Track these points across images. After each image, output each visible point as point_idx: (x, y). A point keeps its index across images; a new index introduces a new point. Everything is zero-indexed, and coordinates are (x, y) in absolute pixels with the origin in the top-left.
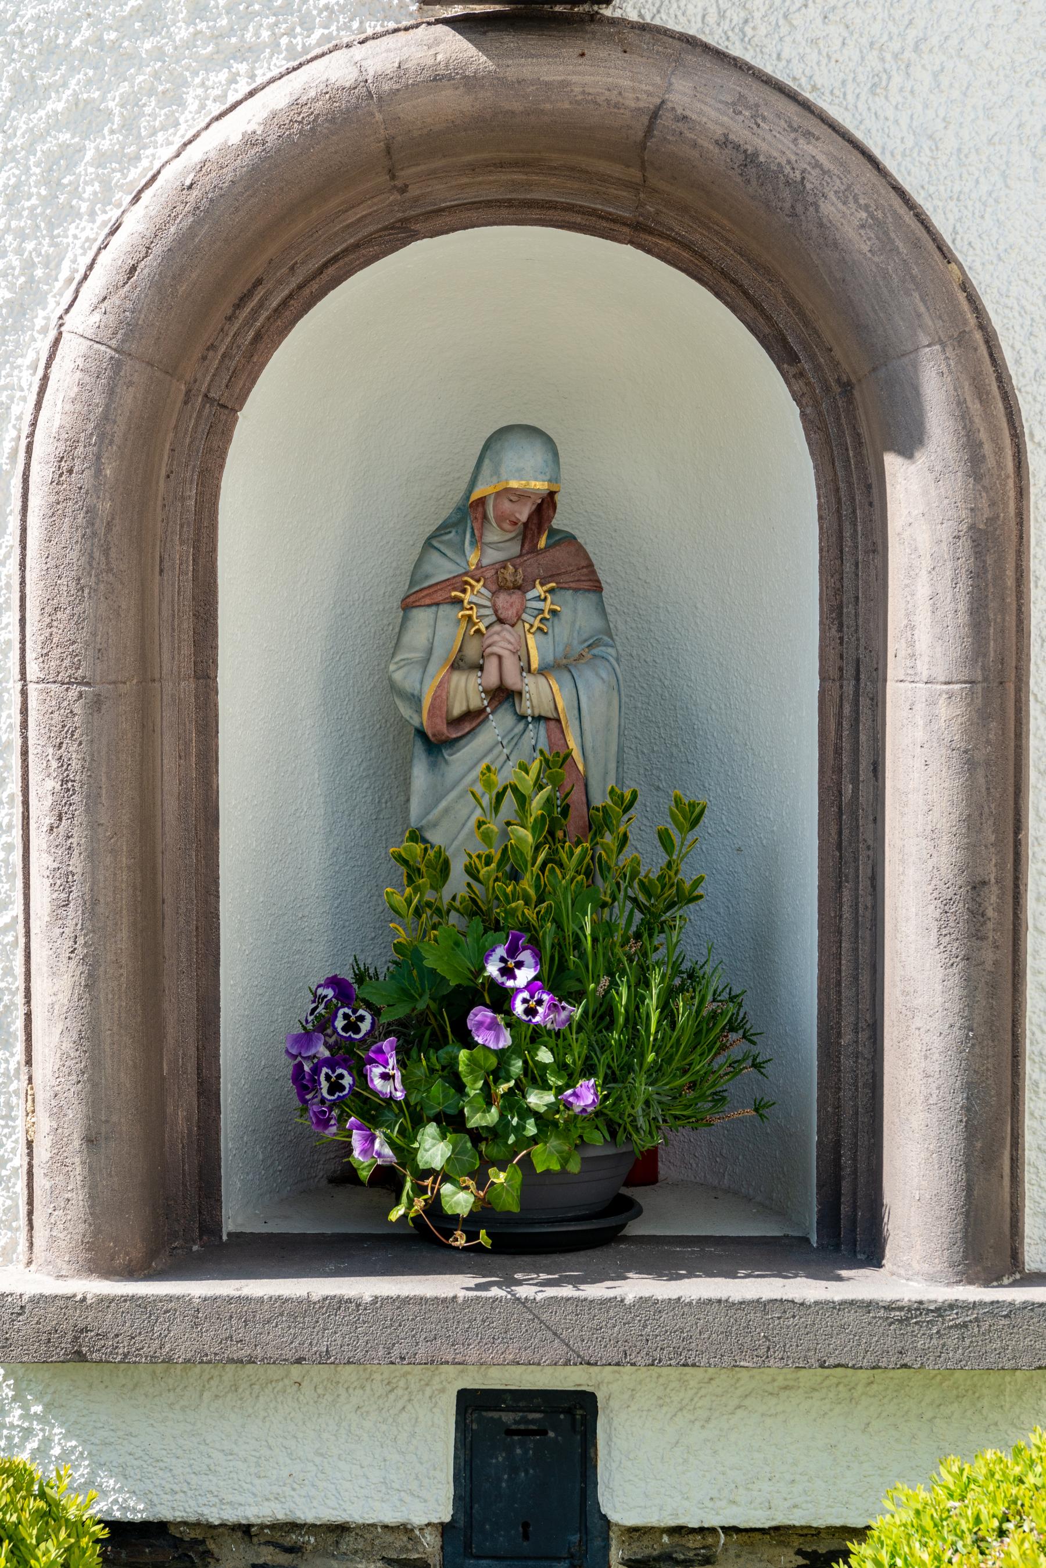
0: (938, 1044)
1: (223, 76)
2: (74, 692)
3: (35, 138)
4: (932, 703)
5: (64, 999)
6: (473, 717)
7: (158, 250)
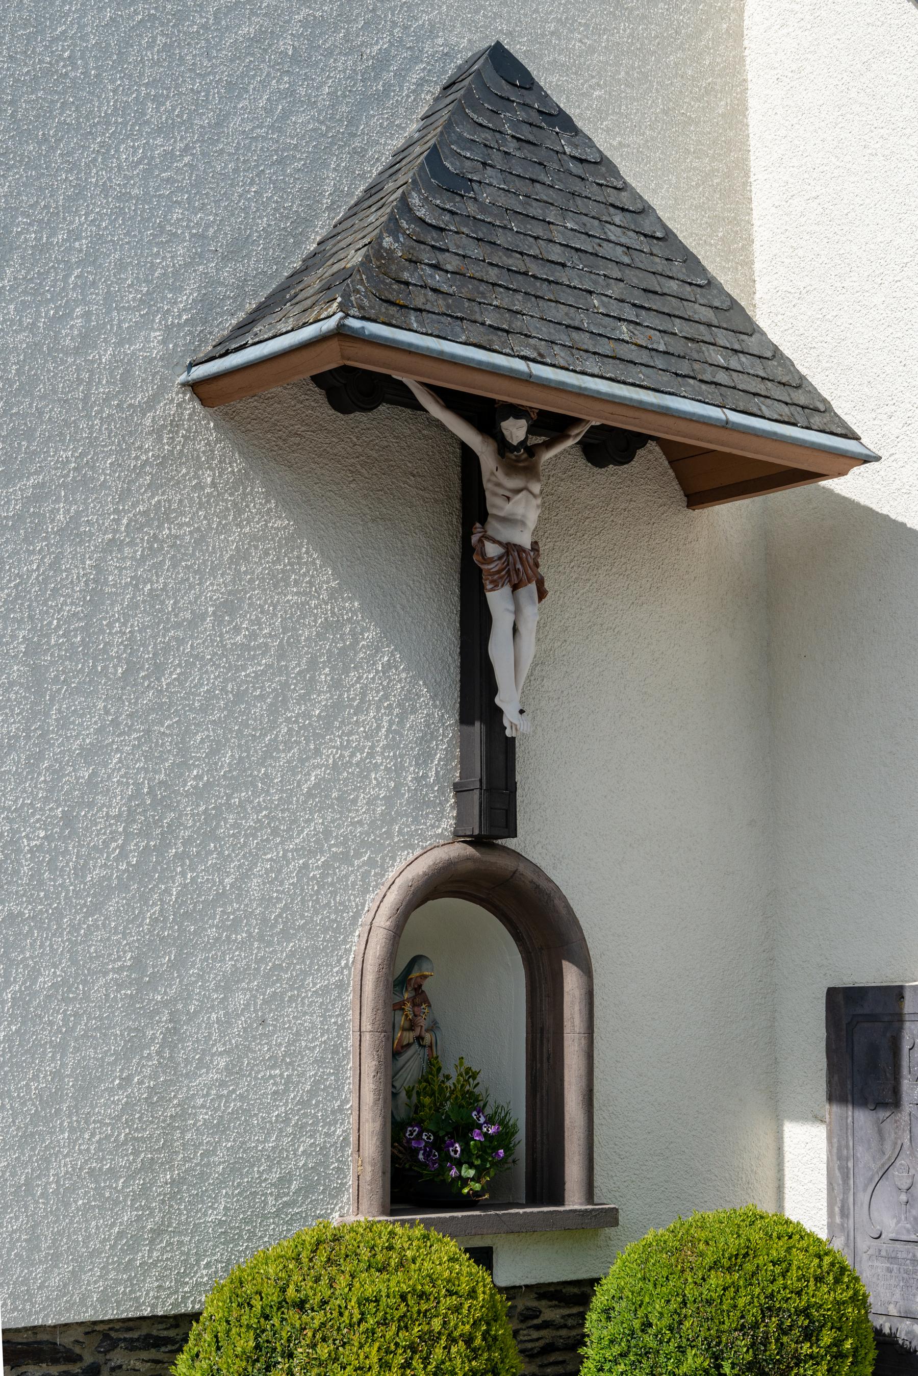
0: (582, 1136)
1: (406, 852)
2: (383, 1034)
3: (359, 867)
4: (580, 1039)
5: (378, 1129)
6: (409, 1045)
7: (404, 904)
